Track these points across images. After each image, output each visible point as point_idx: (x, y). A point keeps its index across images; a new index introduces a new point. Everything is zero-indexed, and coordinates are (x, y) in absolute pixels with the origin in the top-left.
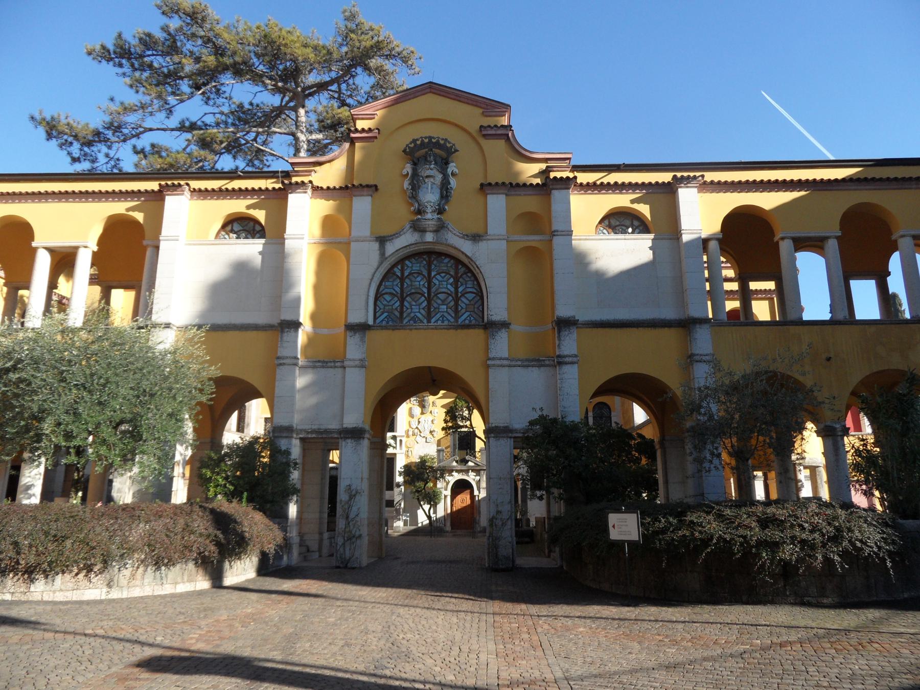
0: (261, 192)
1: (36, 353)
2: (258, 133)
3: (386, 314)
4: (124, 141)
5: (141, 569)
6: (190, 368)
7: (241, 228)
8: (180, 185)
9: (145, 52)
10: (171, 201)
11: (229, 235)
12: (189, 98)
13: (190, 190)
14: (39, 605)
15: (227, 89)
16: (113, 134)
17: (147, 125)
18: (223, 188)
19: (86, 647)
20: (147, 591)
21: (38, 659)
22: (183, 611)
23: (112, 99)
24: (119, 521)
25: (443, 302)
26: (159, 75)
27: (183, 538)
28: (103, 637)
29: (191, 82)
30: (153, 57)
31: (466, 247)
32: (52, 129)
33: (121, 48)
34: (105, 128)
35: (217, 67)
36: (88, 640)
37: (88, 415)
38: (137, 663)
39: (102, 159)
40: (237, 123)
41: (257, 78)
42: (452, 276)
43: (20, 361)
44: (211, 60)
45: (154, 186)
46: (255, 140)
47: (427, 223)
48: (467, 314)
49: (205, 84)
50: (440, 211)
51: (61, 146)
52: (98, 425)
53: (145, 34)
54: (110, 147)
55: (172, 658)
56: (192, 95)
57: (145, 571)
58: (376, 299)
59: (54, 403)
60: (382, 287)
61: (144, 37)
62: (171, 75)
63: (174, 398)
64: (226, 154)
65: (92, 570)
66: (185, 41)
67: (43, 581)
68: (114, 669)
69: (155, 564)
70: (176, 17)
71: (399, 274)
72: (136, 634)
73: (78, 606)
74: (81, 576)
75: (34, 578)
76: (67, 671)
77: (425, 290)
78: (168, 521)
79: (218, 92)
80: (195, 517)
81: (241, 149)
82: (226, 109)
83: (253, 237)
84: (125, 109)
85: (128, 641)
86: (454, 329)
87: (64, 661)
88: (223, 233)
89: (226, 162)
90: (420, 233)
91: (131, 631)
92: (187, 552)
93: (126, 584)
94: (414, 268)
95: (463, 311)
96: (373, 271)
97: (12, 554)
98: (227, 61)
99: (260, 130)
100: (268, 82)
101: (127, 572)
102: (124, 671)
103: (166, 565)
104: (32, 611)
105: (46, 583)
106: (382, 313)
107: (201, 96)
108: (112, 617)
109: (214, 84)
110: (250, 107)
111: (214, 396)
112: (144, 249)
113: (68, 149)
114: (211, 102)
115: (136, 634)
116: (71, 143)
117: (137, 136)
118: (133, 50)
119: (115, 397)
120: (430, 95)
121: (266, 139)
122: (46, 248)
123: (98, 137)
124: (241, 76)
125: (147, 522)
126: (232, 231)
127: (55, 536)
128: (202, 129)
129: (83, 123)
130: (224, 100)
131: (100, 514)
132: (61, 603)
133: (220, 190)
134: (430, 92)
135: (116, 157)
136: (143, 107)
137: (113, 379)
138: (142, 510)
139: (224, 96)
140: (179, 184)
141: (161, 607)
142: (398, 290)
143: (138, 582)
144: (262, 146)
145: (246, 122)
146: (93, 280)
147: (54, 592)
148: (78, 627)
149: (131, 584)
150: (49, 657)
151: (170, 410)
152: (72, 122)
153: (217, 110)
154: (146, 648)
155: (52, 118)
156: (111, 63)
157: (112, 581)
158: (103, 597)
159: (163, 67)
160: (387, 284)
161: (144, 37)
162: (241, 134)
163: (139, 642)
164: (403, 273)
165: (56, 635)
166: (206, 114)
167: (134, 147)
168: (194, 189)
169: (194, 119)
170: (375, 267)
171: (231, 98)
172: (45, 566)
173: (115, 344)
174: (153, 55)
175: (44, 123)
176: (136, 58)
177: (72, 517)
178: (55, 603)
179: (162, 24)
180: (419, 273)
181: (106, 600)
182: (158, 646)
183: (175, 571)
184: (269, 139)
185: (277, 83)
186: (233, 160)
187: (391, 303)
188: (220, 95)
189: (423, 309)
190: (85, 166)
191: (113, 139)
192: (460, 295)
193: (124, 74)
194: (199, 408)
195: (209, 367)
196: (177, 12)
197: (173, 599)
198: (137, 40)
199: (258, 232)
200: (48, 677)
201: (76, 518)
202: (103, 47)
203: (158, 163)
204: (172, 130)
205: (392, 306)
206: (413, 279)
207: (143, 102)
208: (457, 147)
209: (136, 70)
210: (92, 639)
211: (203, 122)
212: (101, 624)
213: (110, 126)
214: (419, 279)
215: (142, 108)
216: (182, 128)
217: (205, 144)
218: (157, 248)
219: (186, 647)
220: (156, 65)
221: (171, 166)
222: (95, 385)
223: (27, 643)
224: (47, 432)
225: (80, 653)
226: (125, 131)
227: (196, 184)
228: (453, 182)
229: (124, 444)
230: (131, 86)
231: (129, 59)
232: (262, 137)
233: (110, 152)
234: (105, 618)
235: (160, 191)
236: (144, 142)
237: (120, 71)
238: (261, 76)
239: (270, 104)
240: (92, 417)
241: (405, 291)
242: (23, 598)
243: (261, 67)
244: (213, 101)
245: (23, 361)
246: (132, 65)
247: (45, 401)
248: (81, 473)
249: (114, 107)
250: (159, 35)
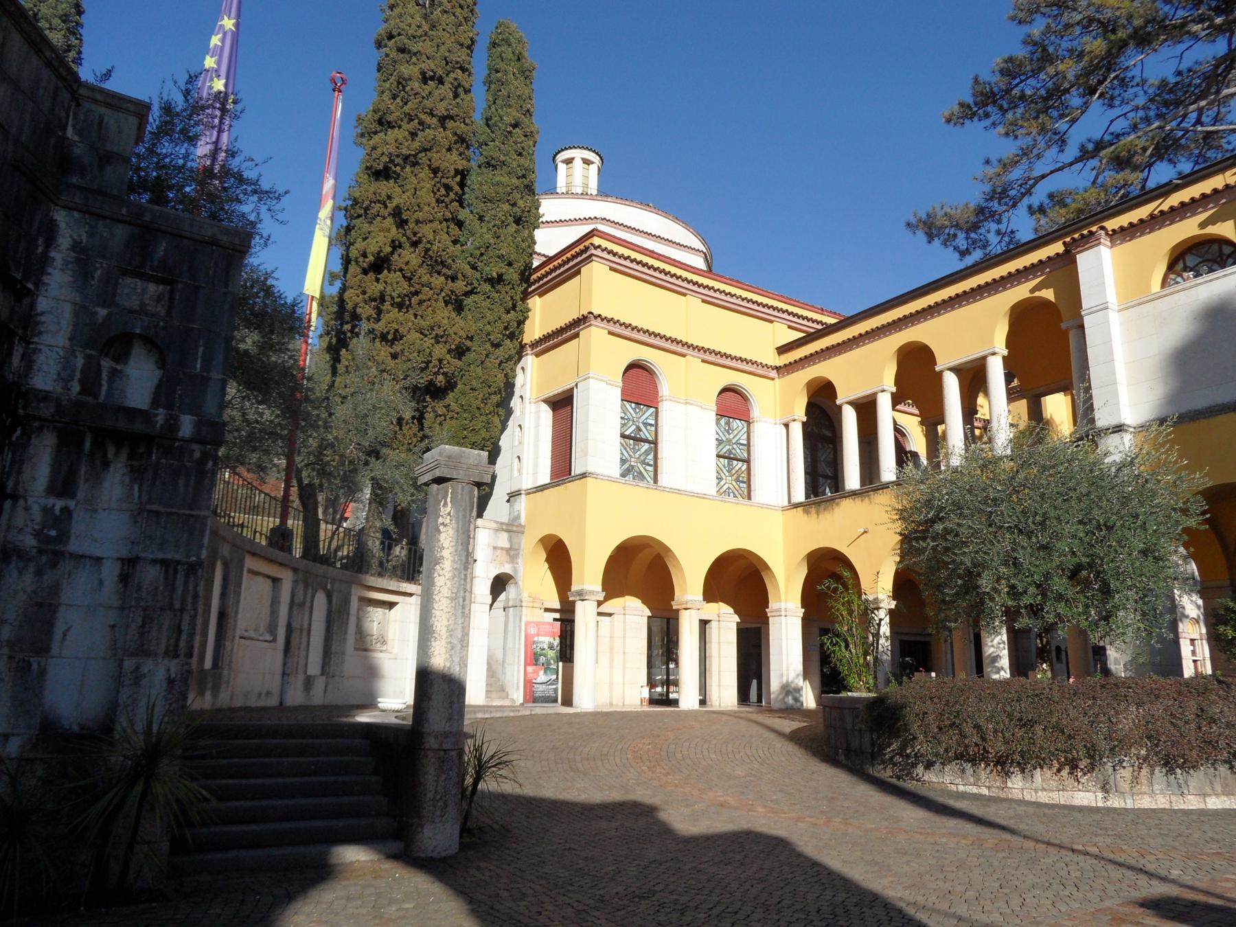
0: (1218, 195)
1: (956, 496)
2: (1200, 111)
4: (1014, 205)
5: (1145, 771)
6: (1159, 481)
7: (1200, 260)
8: (1091, 233)
9: (1011, 84)
10: (1085, 261)
11: (1181, 276)
12: (1082, 113)
13: (1107, 234)
14: (1019, 805)
15: (1136, 72)
16: (1000, 204)
17: (1036, 173)
18: (1156, 212)
19: (1072, 867)
20: (1162, 802)
21: (1013, 872)
22: (1216, 837)
23: (987, 162)
24: (1099, 702)
26: (1036, 103)
27: (1200, 728)
28: (1096, 857)
29: (1081, 90)
30: (1021, 85)
32: (931, 228)
33: (982, 94)
34: (987, 200)
35: (1109, 52)
36: (1076, 858)
37: (1030, 564)
38: (1141, 901)
39: (993, 239)
40: (1164, 110)
41: (1177, 32)
43: (942, 509)
44: (1096, 45)
45: (1057, 248)
46: (1199, 122)
49: (1100, 83)
51: (945, 244)
52: (1047, 576)
53: (1006, 61)
54: (999, 222)
55: (1194, 904)
56: (1086, 105)
57: (1152, 773)
59: (988, 554)
61: (1005, 65)
62: (1053, 95)
63: (1144, 527)
64: (1158, 163)
65: (1077, 767)
66: (1058, 41)
67: (1020, 776)
68: (1107, 904)
69: (1165, 765)
70: (1038, 16)
72: (1142, 861)
73: (1066, 812)
74: (1065, 773)
75: (1009, 771)
76: (1047, 894)
78: (1170, 703)
79: (1123, 83)
80: (1213, 697)
81: (1180, 145)
82: (1141, 101)
83: (1223, 266)
84: (1005, 165)
85: (1129, 867)
87: (1044, 880)
88: (1172, 276)
89: (1162, 173)
91: (1135, 854)
92: (1210, 749)
93: (1128, 789)
97: (976, 739)
98: (1121, 34)
99: (1203, 103)
100: (1196, 28)
101: (1126, 773)
102: (1121, 909)
103: (1182, 767)
104: (1011, 812)
105: (1024, 779)
107: (1101, 101)
108: (1110, 832)
109: (1113, 75)
110: (1178, 79)
111: (1208, 515)
112: (1066, 333)
113: (954, 243)
114: (1117, 102)
115: (1142, 861)
116: (955, 236)
117: (1029, 192)
118: (995, 89)
119: (1057, 536)
121: (1218, 113)
122: (951, 369)
123: (984, 214)
124: (1149, 43)
125: (1138, 705)
126: (1186, 269)
127: (1020, 720)
128: (1112, 144)
129: (961, 207)
130: (1135, 89)
131: (1072, 692)
132: (1046, 805)
133: (1152, 216)
135: (1009, 230)
136: (1025, 152)
137: (1052, 513)
138: (1130, 688)
139: (1134, 83)
140: (1090, 232)
141: (1183, 827)
143: (1145, 788)
144: (1214, 125)
145: (1178, 103)
146: (1012, 396)
147: (1036, 791)
148: (1064, 839)
149: (1135, 790)
150: (1026, 872)
151: (1142, 545)
152: (949, 210)
153: (1127, 108)
154: (1154, 882)
155: (928, 215)
156: (976, 119)
157: (1108, 783)
158: (1100, 804)
159: (1038, 90)
161: (1005, 65)
162: (1174, 124)
163: (1146, 872)
165: (1037, 846)
166: (1112, 121)
167: (1030, 207)
168: (1113, 230)
169: (1097, 136)
171: (1144, 81)
172: (1017, 757)
173: (1044, 468)
174: (1022, 81)
175: (921, 225)
176: (1002, 97)
177: (1037, 695)
178: (1038, 805)
179: (1022, 37)
181: (1104, 808)
182: (1173, 881)
183: (1197, 778)
184: (1223, 110)
185: (1213, 20)
186: (1172, 166)
188: (1127, 86)
190: (977, 255)
191: (1001, 209)
193: (994, 125)
194: (1186, 537)
195: (1189, 475)
196: (1037, 10)
197: (1202, 818)
198: (998, 74)
199: (1229, 256)
200: (1023, 896)
201: (1042, 696)
202: (962, 105)
203: (1059, 216)
204: (1071, 164)
207: (1024, 147)
209: (1006, 111)
210: (1081, 857)
211: (1112, 134)
212: (1095, 839)
213: (994, 195)
215: (1025, 154)
216: (1085, 155)
217: (1121, 162)
218: (1082, 327)
219: (1219, 891)
220: (1029, 92)
221: (1080, 211)
222: (1031, 525)
223: (1003, 850)
224: (987, 590)
225: (1064, 873)
226: (1013, 193)
227: (1113, 224)
229: (1088, 598)
230: (1007, 134)
231: (994, 102)
232: (1210, 113)
233: (1000, 226)
234: (1100, 832)
235: (1067, 251)
236: (1039, 195)
237: (987, 122)
238: (1184, 25)
239: (1210, 59)
240: (1037, 566)
242: (1002, 795)
243: (1181, 13)
244: (1119, 99)
245: (945, 508)
246: (1001, 108)
247: (977, 552)
248: (1045, 640)
249: (991, 171)
250: (1021, 52)
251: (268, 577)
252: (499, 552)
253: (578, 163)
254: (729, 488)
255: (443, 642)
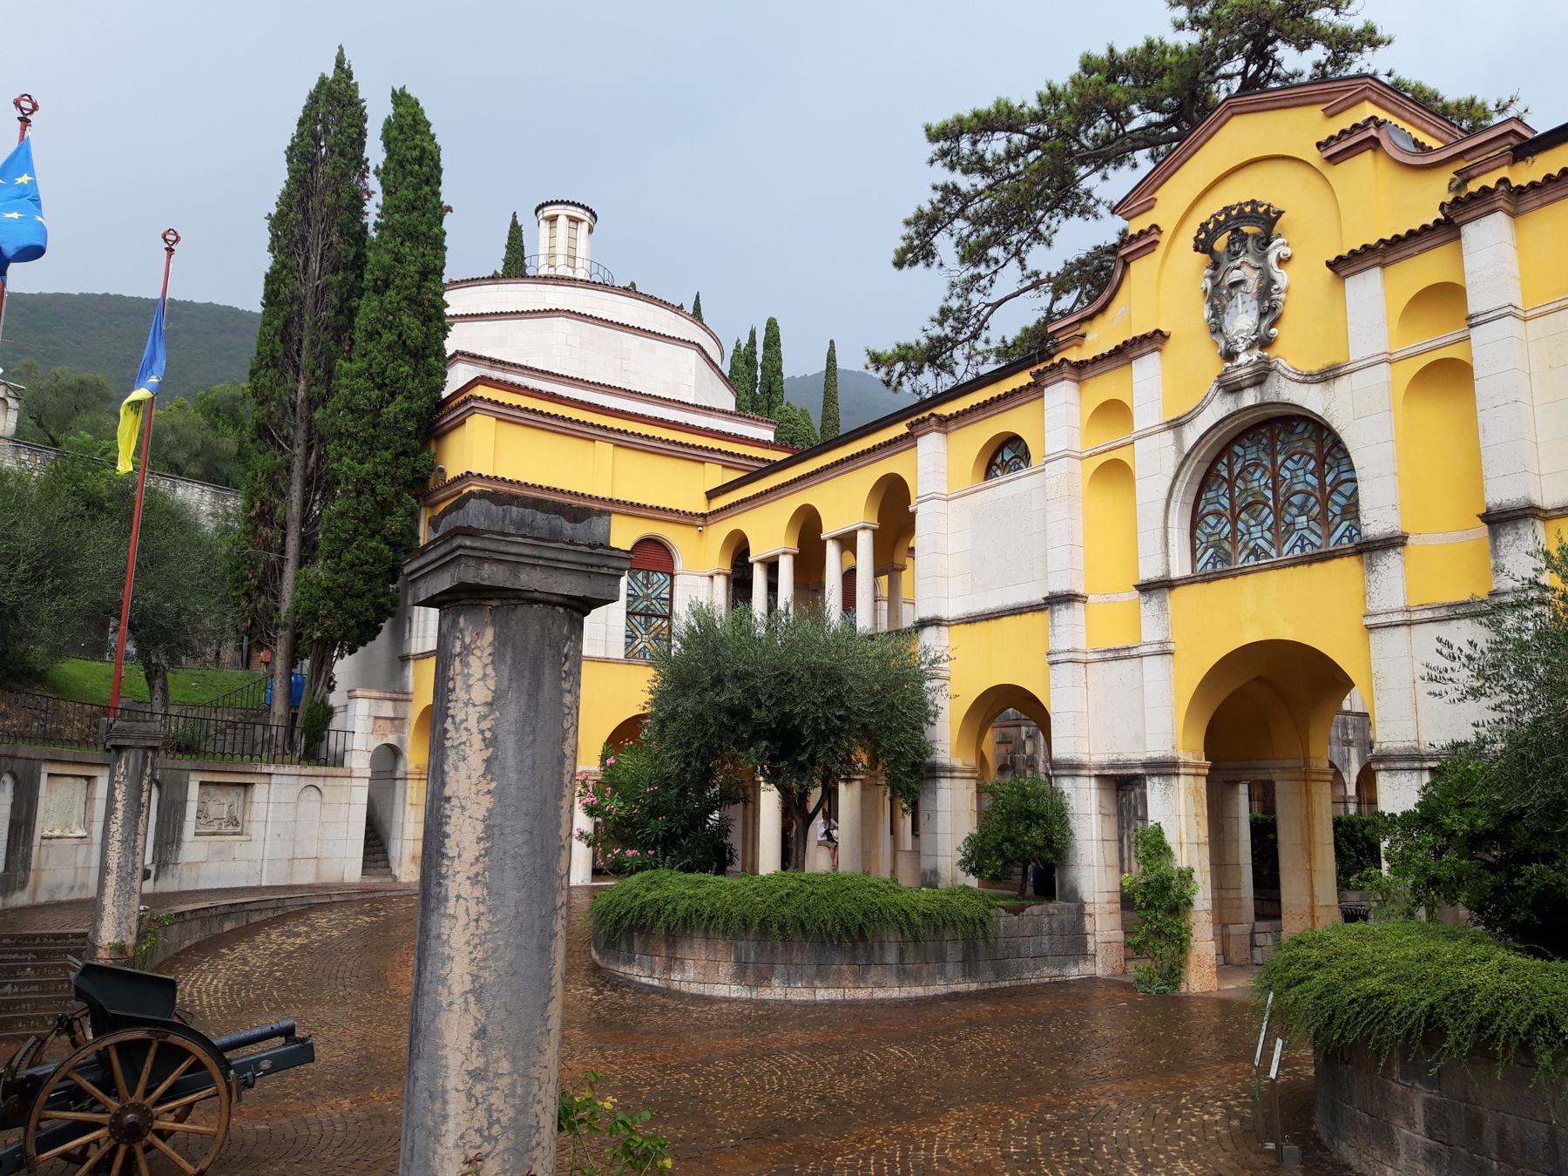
3: (1211, 551)
25: (1302, 510)
31: (1311, 399)
42: (1312, 456)
47: (1238, 373)
48: (1346, 523)
50: (1265, 342)
58: (1194, 526)
60: (1202, 503)
71: (1225, 474)
77: (1269, 494)
86: (1538, 509)
90: (1234, 396)
94: (1248, 457)
95: (1337, 520)
96: (1169, 482)
106: (1206, 550)
120: (1235, 120)
122: (833, 538)
134: (1233, 115)
142: (1225, 502)
160: (1210, 495)
164: (1230, 472)
170: (1171, 475)
180: (1257, 465)
187: (1217, 530)
189: (1269, 530)
192: (1328, 489)
205: (1219, 533)
206: (1249, 477)
208: (1277, 206)
214: (1257, 475)
228: (1282, 277)
241: (1238, 502)
251: (81, 777)
252: (381, 722)
253: (562, 220)
254: (645, 647)
255: (114, 876)
